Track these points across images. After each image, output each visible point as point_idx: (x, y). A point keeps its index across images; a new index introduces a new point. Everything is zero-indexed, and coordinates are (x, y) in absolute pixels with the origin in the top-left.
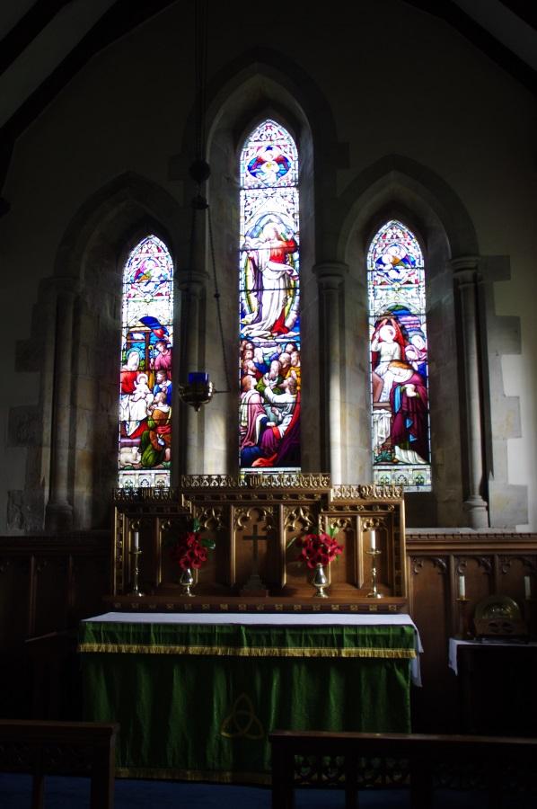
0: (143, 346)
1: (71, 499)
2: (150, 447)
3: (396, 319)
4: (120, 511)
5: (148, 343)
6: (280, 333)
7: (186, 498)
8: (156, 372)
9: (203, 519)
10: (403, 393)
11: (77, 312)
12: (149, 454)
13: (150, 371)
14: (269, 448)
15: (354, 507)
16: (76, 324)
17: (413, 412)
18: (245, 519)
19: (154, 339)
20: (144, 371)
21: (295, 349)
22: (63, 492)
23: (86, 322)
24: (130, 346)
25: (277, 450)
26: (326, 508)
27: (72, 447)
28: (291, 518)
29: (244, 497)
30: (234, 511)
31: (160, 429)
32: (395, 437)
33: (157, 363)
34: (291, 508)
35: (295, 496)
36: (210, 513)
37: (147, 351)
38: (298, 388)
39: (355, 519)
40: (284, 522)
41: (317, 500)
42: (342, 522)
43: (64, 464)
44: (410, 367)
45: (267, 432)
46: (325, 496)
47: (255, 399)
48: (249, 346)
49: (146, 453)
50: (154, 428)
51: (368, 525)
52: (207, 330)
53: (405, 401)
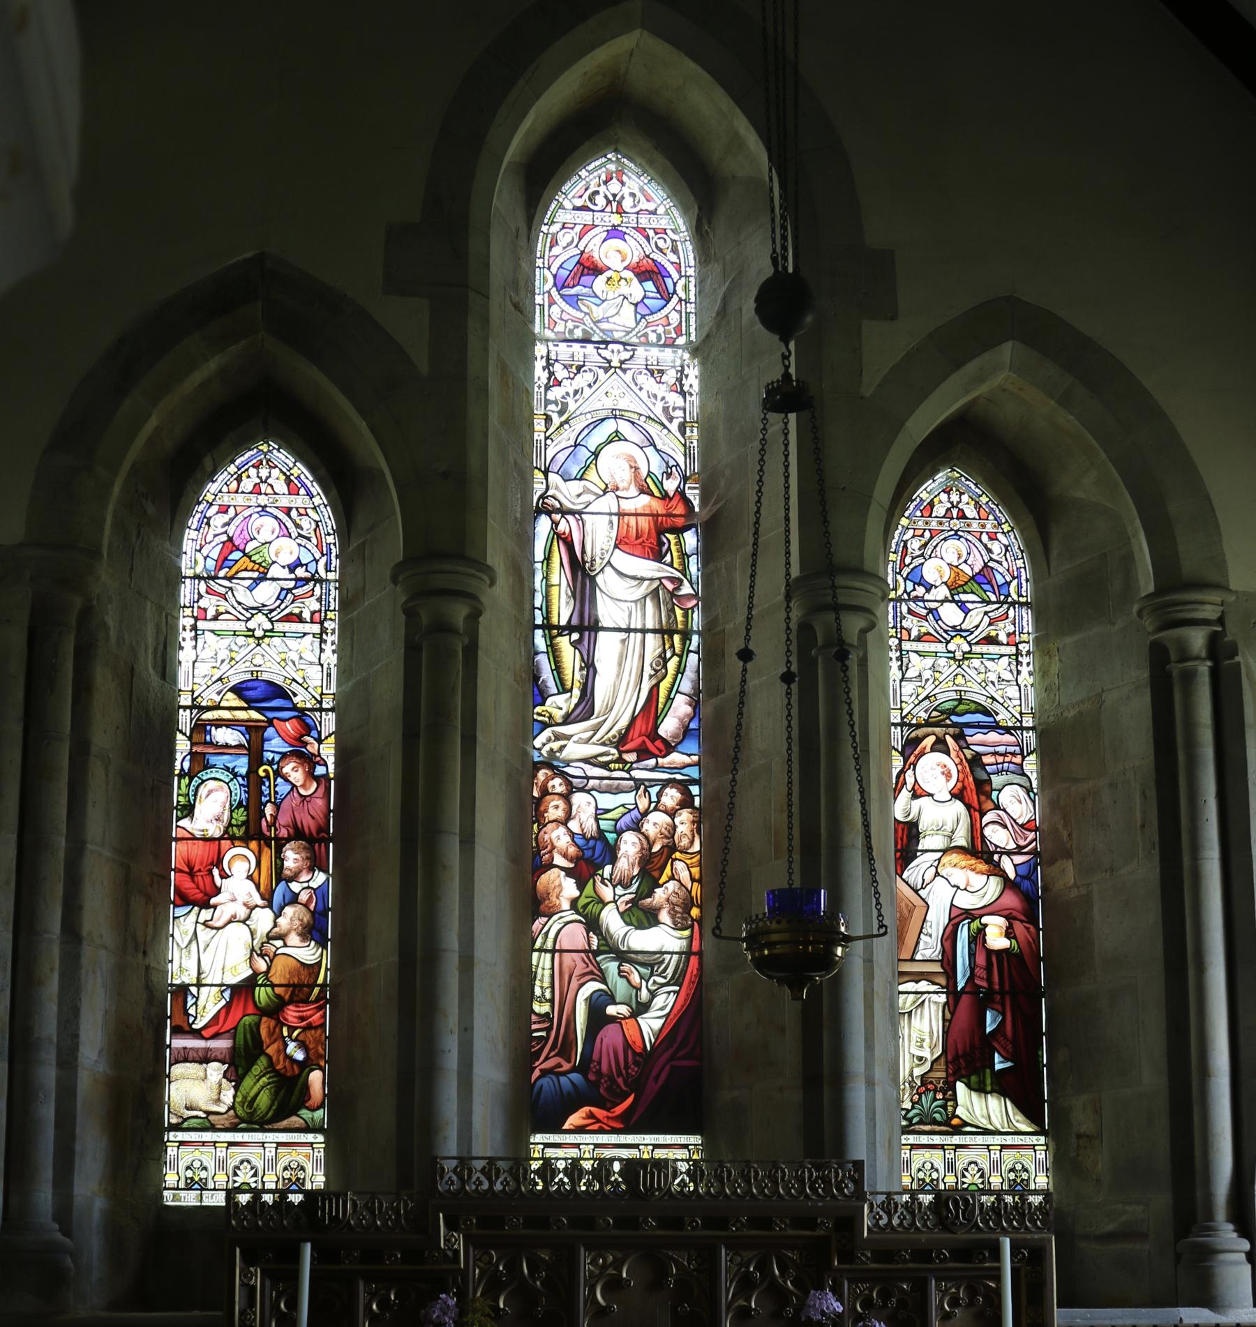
0: (242, 765)
1: (64, 1212)
2: (263, 1061)
3: (959, 737)
4: (248, 1260)
5: (256, 758)
6: (643, 754)
7: (451, 1225)
8: (280, 845)
9: (494, 1285)
10: (978, 937)
11: (84, 654)
12: (258, 1084)
13: (264, 840)
14: (611, 1078)
15: (923, 1254)
16: (83, 688)
17: (1002, 992)
18: (614, 1286)
19: (275, 745)
20: (245, 840)
21: (686, 802)
22: (44, 1196)
23: (104, 682)
24: (200, 762)
25: (636, 1085)
26: (848, 1256)
27: (68, 1060)
28: (746, 1285)
29: (619, 1223)
30: (586, 1264)
31: (291, 1013)
32: (956, 1058)
33: (284, 819)
34: (747, 1255)
35: (764, 1222)
36: (513, 1267)
37: (253, 782)
38: (695, 912)
39: (921, 1288)
40: (728, 1291)
41: (820, 1232)
42: (885, 1295)
43: (47, 1112)
44: (997, 870)
45: (609, 1035)
46: (849, 1222)
47: (575, 936)
48: (557, 785)
49: (248, 1082)
50: (274, 1011)
51: (954, 1302)
52: (480, 737)
53: (981, 960)
